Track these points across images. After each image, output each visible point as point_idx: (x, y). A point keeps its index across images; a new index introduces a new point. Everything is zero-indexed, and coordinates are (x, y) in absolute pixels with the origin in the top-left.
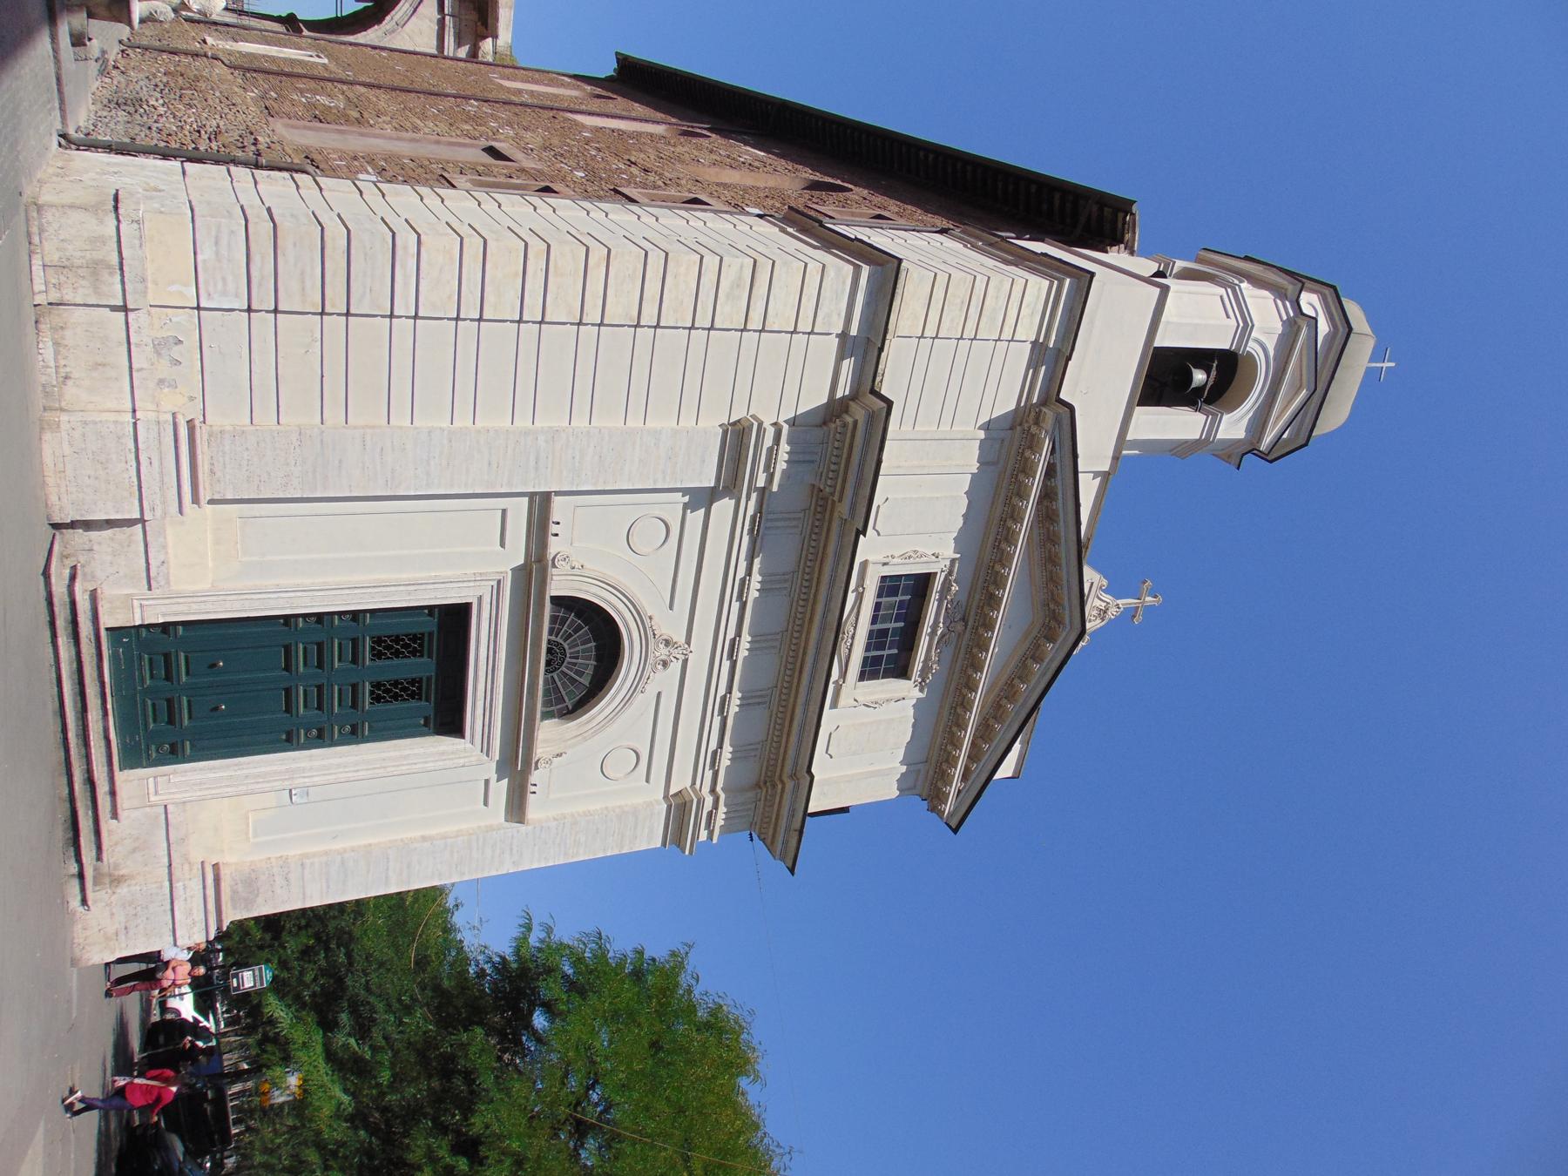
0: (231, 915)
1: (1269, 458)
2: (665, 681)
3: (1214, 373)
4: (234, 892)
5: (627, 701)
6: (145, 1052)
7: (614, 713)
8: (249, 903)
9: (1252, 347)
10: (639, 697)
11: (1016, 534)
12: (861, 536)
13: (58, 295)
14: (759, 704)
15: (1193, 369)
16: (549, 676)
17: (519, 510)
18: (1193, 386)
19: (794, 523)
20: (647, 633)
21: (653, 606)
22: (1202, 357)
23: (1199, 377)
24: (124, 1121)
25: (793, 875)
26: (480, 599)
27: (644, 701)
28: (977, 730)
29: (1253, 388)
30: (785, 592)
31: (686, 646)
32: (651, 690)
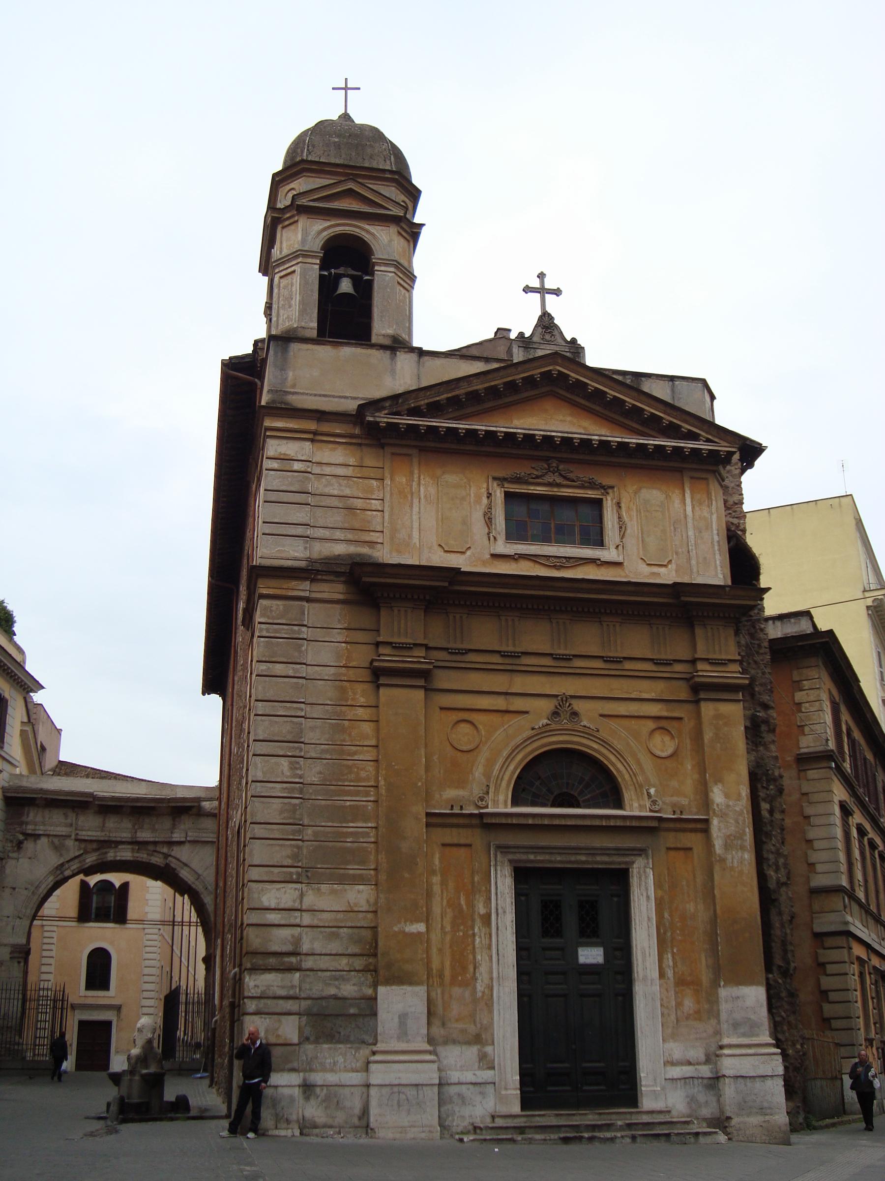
0: (766, 1038)
3: (341, 271)
4: (744, 1035)
5: (604, 743)
7: (543, 735)
9: (316, 245)
10: (603, 734)
11: (675, 448)
15: (354, 293)
16: (582, 804)
18: (354, 293)
20: (544, 731)
22: (327, 286)
23: (346, 286)
24: (39, 747)
25: (769, 589)
27: (607, 729)
28: (669, 437)
29: (355, 236)
31: (559, 698)
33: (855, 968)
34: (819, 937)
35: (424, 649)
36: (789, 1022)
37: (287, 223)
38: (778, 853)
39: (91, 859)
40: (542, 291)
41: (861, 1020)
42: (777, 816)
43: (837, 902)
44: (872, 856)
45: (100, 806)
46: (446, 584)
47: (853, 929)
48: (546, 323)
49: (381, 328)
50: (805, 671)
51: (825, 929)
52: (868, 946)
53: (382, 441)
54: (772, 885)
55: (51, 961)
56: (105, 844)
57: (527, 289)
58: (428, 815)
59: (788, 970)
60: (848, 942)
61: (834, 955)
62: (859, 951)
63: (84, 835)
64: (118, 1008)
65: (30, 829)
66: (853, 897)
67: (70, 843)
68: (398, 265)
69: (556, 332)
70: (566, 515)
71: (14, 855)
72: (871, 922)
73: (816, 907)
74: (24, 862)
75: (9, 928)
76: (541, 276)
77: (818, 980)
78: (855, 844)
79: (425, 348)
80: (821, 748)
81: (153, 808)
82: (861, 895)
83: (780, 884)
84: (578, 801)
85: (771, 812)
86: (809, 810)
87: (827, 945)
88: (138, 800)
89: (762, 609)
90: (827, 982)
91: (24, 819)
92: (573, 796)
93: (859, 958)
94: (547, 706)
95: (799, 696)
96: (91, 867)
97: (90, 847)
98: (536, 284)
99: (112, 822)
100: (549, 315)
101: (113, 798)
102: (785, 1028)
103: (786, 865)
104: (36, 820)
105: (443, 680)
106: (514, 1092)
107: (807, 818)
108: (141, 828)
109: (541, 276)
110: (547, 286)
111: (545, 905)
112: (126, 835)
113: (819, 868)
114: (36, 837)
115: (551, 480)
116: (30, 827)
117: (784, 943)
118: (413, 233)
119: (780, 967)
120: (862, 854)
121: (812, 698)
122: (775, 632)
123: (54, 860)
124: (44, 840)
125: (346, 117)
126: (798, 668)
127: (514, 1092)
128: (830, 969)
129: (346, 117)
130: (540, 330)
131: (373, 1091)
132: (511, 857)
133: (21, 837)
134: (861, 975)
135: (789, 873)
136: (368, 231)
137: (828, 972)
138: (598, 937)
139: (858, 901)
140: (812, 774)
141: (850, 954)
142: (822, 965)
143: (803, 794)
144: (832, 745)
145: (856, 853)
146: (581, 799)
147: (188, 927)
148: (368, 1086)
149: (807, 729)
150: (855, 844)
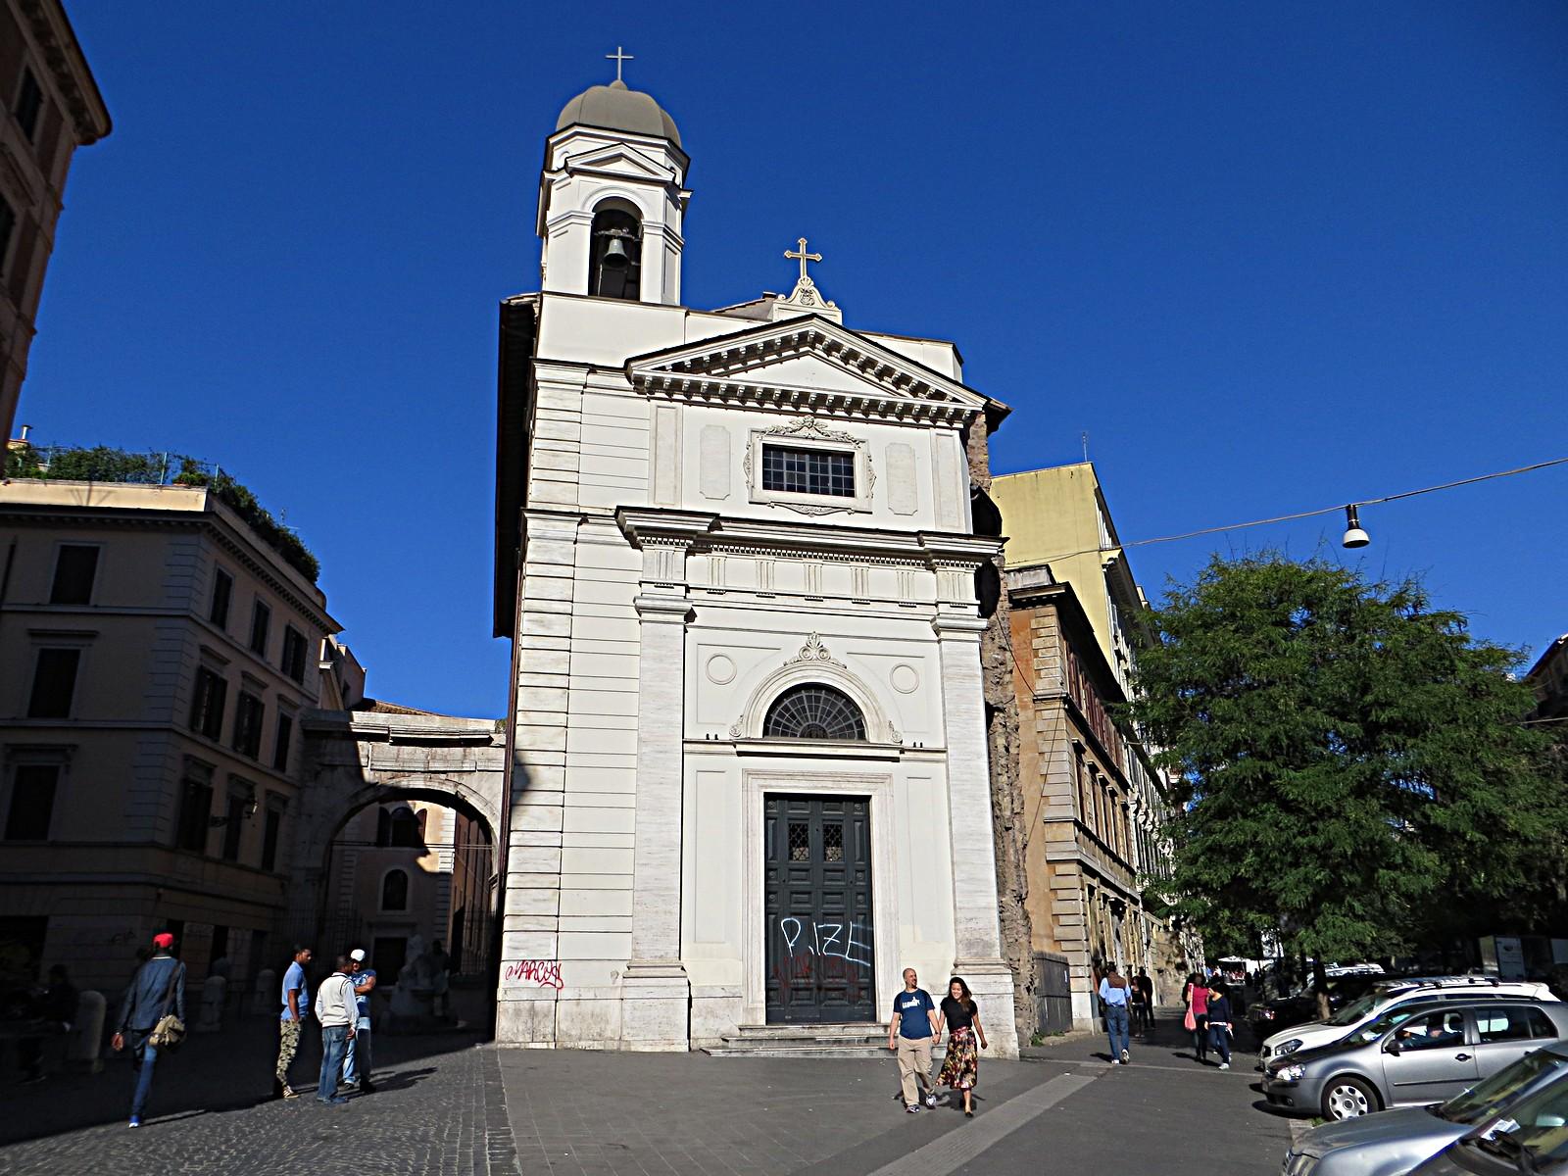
8: (988, 945)
65: (327, 760)
114: (333, 767)
124: (340, 770)
132: (762, 782)
133: (319, 768)
135: (1023, 803)
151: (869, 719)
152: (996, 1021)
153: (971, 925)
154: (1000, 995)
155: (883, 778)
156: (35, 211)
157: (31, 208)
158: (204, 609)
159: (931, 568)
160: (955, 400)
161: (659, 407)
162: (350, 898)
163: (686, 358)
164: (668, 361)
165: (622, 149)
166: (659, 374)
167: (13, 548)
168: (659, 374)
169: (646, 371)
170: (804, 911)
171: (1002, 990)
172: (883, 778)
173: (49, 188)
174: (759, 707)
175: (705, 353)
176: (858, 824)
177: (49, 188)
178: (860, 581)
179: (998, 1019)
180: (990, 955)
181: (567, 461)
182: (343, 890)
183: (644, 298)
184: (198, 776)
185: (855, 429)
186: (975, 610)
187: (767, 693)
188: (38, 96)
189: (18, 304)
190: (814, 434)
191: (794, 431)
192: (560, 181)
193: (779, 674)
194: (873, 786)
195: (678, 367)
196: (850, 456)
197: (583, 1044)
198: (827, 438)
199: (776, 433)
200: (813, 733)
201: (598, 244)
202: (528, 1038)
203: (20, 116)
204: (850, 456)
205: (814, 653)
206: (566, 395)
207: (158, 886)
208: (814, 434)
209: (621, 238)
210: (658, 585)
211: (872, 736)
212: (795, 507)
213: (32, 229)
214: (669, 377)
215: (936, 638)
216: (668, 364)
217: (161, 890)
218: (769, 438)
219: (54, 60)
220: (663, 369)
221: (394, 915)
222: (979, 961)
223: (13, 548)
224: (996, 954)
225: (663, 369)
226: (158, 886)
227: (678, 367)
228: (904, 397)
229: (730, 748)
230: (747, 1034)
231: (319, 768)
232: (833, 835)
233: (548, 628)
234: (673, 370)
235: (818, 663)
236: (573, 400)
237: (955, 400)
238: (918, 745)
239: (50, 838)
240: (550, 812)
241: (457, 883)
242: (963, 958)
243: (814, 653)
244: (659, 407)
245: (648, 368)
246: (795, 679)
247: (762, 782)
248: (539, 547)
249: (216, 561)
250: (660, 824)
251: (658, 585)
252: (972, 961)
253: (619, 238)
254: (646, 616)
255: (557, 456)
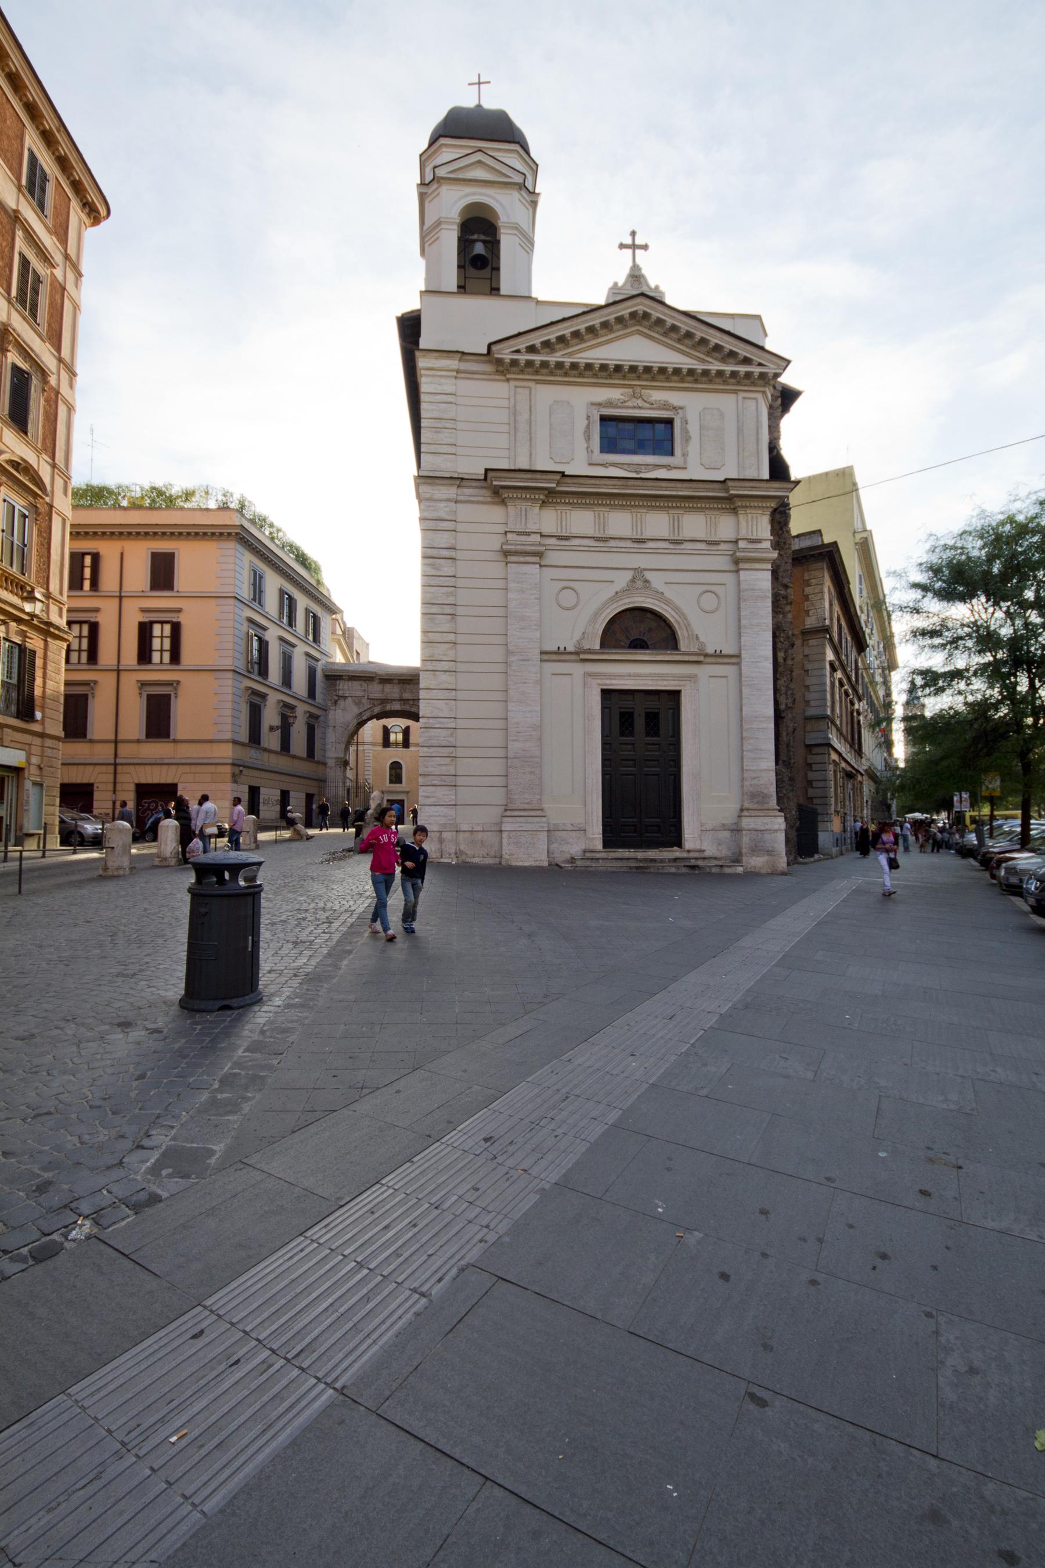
1: (535, 168)
2: (657, 580)
3: (475, 237)
4: (758, 802)
6: (211, 1150)
8: (766, 797)
12: (620, 284)
13: (453, 542)
14: (679, 520)
17: (550, 667)
19: (564, 515)
21: (609, 592)
26: (599, 684)
27: (669, 593)
30: (606, 514)
32: (661, 588)
33: (831, 767)
34: (809, 747)
35: (539, 536)
36: (788, 798)
37: (432, 197)
38: (788, 688)
39: (377, 710)
40: (634, 247)
41: (833, 799)
42: (790, 662)
43: (822, 725)
44: (846, 700)
45: (380, 679)
46: (554, 485)
47: (832, 742)
48: (636, 275)
49: (507, 283)
50: (813, 572)
51: (813, 743)
52: (840, 754)
53: (508, 376)
54: (783, 707)
55: (370, 769)
56: (384, 701)
57: (622, 246)
58: (542, 653)
59: (790, 763)
60: (829, 751)
61: (818, 759)
62: (834, 756)
63: (372, 696)
64: (408, 793)
65: (341, 693)
66: (833, 722)
67: (365, 701)
68: (517, 228)
69: (642, 280)
70: (645, 432)
71: (333, 708)
72: (842, 741)
73: (808, 728)
74: (339, 712)
75: (334, 749)
76: (633, 234)
77: (806, 774)
78: (837, 690)
79: (540, 299)
80: (821, 624)
81: (411, 680)
82: (838, 723)
83: (788, 708)
84: (646, 644)
85: (785, 660)
86: (808, 666)
87: (813, 752)
88: (402, 675)
89: (788, 532)
90: (811, 776)
91: (337, 687)
92: (644, 641)
93: (834, 761)
94: (629, 575)
95: (808, 590)
96: (377, 714)
97: (376, 702)
98: (628, 241)
99: (388, 688)
100: (638, 266)
101: (387, 675)
102: (785, 800)
103: (792, 694)
104: (344, 687)
105: (552, 558)
106: (598, 836)
107: (807, 671)
108: (405, 691)
109: (633, 234)
110: (637, 242)
111: (622, 714)
112: (396, 696)
113: (812, 703)
114: (345, 698)
115: (635, 404)
116: (341, 692)
117: (788, 745)
118: (532, 198)
119: (784, 761)
120: (840, 697)
121: (817, 591)
122: (796, 545)
123: (356, 710)
124: (350, 699)
125: (479, 106)
126: (808, 571)
127: (598, 836)
128: (814, 767)
129: (479, 106)
130: (630, 279)
131: (505, 835)
132: (599, 681)
133: (336, 698)
134: (835, 771)
135: (794, 700)
136: (491, 197)
137: (814, 769)
138: (658, 736)
139: (836, 726)
140: (812, 642)
141: (829, 758)
142: (810, 765)
143: (805, 656)
144: (827, 622)
145: (837, 696)
146: (649, 643)
147: (164, 648)
148: (501, 831)
149: (811, 613)
150: (837, 690)
151: (681, 634)
152: (770, 849)
153: (755, 782)
154: (776, 831)
155: (692, 678)
156: (58, 273)
157: (54, 271)
158: (245, 592)
159: (734, 511)
160: (760, 364)
161: (516, 387)
162: (370, 777)
163: (537, 339)
164: (522, 344)
165: (479, 156)
166: (516, 356)
167: (122, 554)
168: (516, 356)
169: (505, 353)
170: (528, 548)
171: (776, 827)
172: (692, 678)
173: (67, 257)
174: (597, 626)
175: (552, 335)
176: (671, 711)
177: (67, 257)
178: (676, 526)
179: (773, 847)
180: (768, 803)
181: (445, 437)
182: (366, 773)
183: (503, 292)
184: (257, 700)
185: (675, 398)
186: (767, 545)
187: (603, 615)
188: (45, 178)
189: (58, 349)
190: (640, 402)
191: (625, 402)
192: (432, 193)
193: (612, 600)
194: (681, 683)
195: (531, 349)
196: (670, 422)
197: (476, 860)
198: (652, 405)
199: (609, 404)
200: (638, 644)
201: (464, 244)
202: (439, 855)
203: (32, 193)
204: (670, 422)
205: (639, 584)
206: (443, 381)
207: (240, 766)
208: (640, 402)
209: (484, 242)
210: (519, 533)
211: (683, 646)
212: (626, 467)
213: (60, 289)
214: (523, 358)
215: (733, 568)
216: (522, 347)
217: (241, 768)
218: (604, 410)
219: (48, 138)
220: (518, 351)
221: (396, 787)
222: (760, 807)
223: (122, 554)
224: (773, 802)
225: (518, 351)
226: (240, 766)
227: (531, 349)
228: (715, 366)
229: (574, 657)
230: (588, 855)
231: (336, 698)
232: (652, 720)
233: (439, 570)
234: (526, 352)
235: (643, 591)
236: (448, 386)
237: (760, 364)
238: (718, 652)
239: (172, 737)
240: (446, 704)
241: (676, 853)
242: (746, 805)
243: (639, 584)
244: (516, 387)
245: (507, 351)
246: (625, 604)
247: (599, 681)
248: (429, 507)
249: (251, 562)
250: (525, 712)
251: (519, 533)
252: (755, 806)
253: (481, 241)
254: (511, 558)
255: (439, 432)
